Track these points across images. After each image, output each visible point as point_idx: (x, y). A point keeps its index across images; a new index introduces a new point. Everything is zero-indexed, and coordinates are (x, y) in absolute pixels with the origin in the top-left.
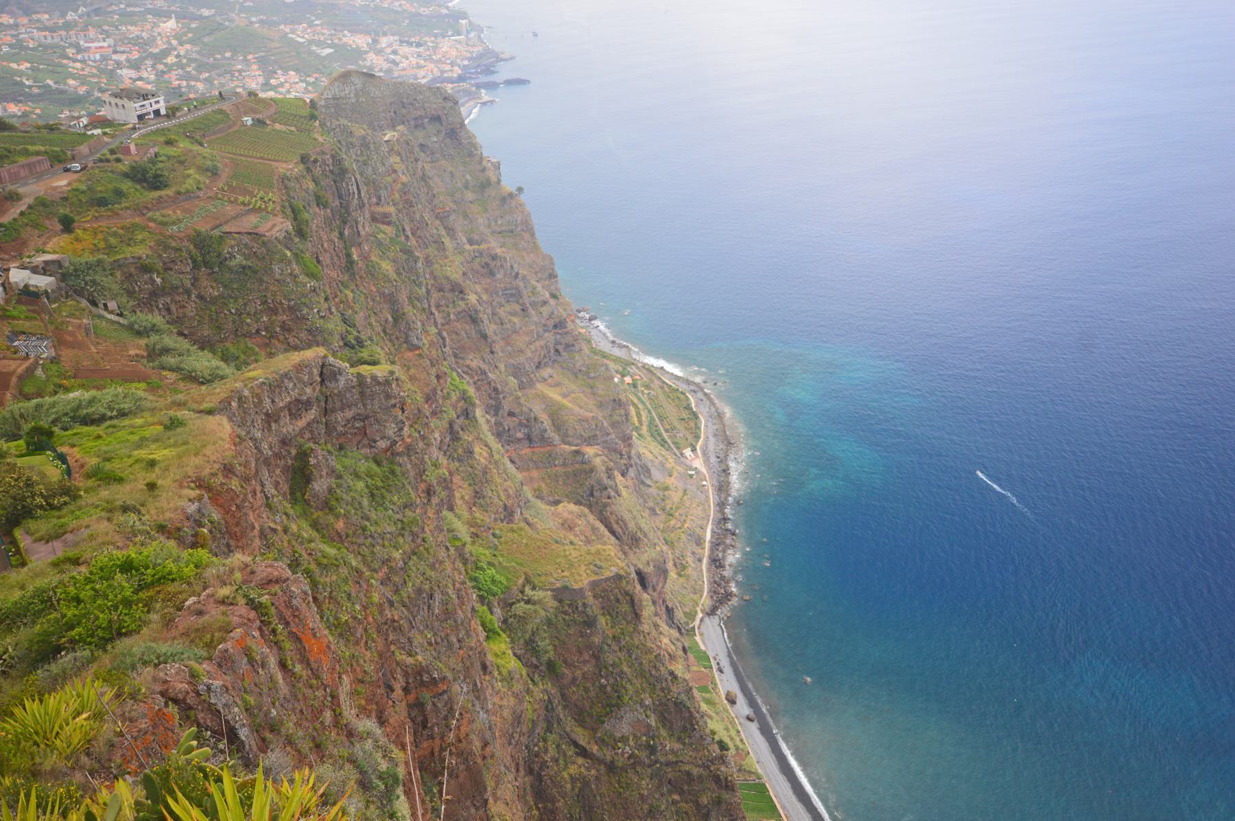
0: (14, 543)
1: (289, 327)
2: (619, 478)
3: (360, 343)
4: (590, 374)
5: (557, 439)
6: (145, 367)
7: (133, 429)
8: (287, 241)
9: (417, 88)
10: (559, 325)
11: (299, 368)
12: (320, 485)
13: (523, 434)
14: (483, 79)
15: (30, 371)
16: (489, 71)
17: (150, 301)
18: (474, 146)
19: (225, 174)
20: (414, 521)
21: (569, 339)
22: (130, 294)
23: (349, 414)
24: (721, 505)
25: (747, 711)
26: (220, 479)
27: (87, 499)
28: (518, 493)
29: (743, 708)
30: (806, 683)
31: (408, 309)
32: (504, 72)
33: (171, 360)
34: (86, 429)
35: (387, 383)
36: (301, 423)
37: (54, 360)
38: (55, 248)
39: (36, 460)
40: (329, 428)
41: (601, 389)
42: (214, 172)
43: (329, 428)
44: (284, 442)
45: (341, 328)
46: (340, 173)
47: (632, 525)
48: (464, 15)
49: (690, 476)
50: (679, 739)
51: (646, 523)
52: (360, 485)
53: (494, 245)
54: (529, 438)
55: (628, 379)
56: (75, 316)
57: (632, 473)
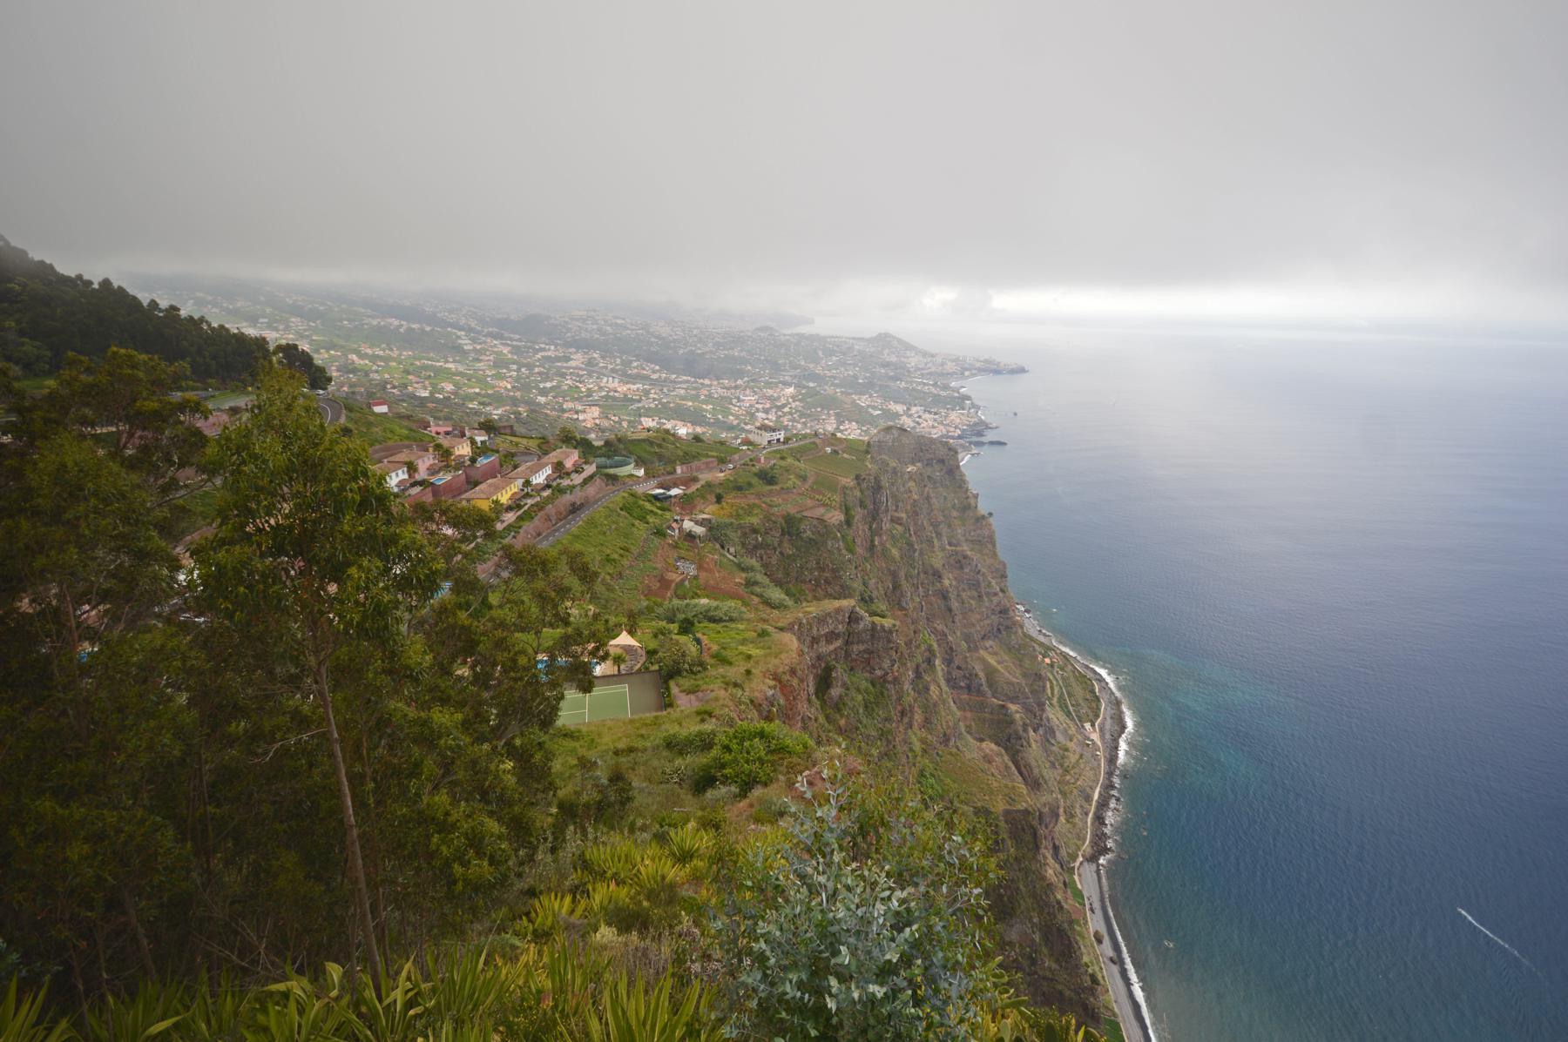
0: (668, 689)
1: (829, 582)
2: (1031, 733)
3: (871, 600)
4: (1022, 650)
5: (989, 693)
6: (742, 590)
7: (738, 631)
8: (839, 527)
9: (932, 441)
10: (1004, 612)
11: (838, 610)
12: (835, 692)
13: (966, 684)
14: (975, 439)
15: (683, 581)
16: (980, 434)
17: (752, 550)
18: (964, 481)
19: (810, 481)
20: (890, 732)
21: (1009, 623)
22: (743, 545)
23: (862, 647)
24: (1110, 774)
25: (1111, 953)
26: (787, 677)
27: (712, 672)
28: (955, 727)
29: (1107, 949)
30: (1168, 949)
31: (903, 582)
32: (990, 436)
33: (757, 589)
34: (712, 625)
35: (891, 632)
36: (831, 647)
37: (696, 577)
38: (709, 511)
39: (683, 639)
40: (847, 655)
41: (1027, 663)
42: (804, 479)
43: (847, 655)
44: (819, 658)
45: (862, 588)
46: (878, 488)
47: (1036, 771)
48: (969, 398)
49: (1085, 743)
50: (1057, 961)
51: (1051, 775)
52: (860, 697)
53: (965, 548)
54: (969, 687)
55: (1047, 661)
56: (712, 555)
57: (1041, 731)
